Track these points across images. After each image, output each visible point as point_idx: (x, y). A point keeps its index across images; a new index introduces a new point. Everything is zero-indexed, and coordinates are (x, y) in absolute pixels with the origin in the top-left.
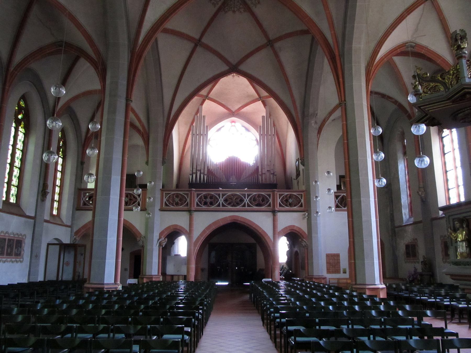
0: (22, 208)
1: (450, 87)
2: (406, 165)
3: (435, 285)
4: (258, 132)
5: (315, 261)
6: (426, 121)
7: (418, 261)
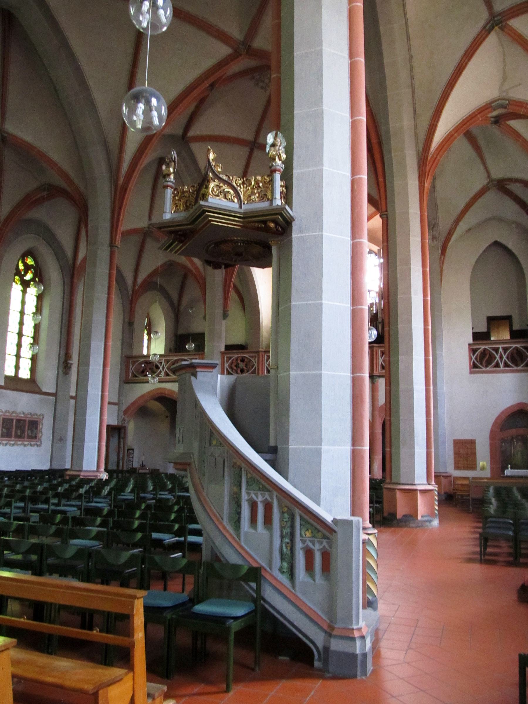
0: (37, 383)
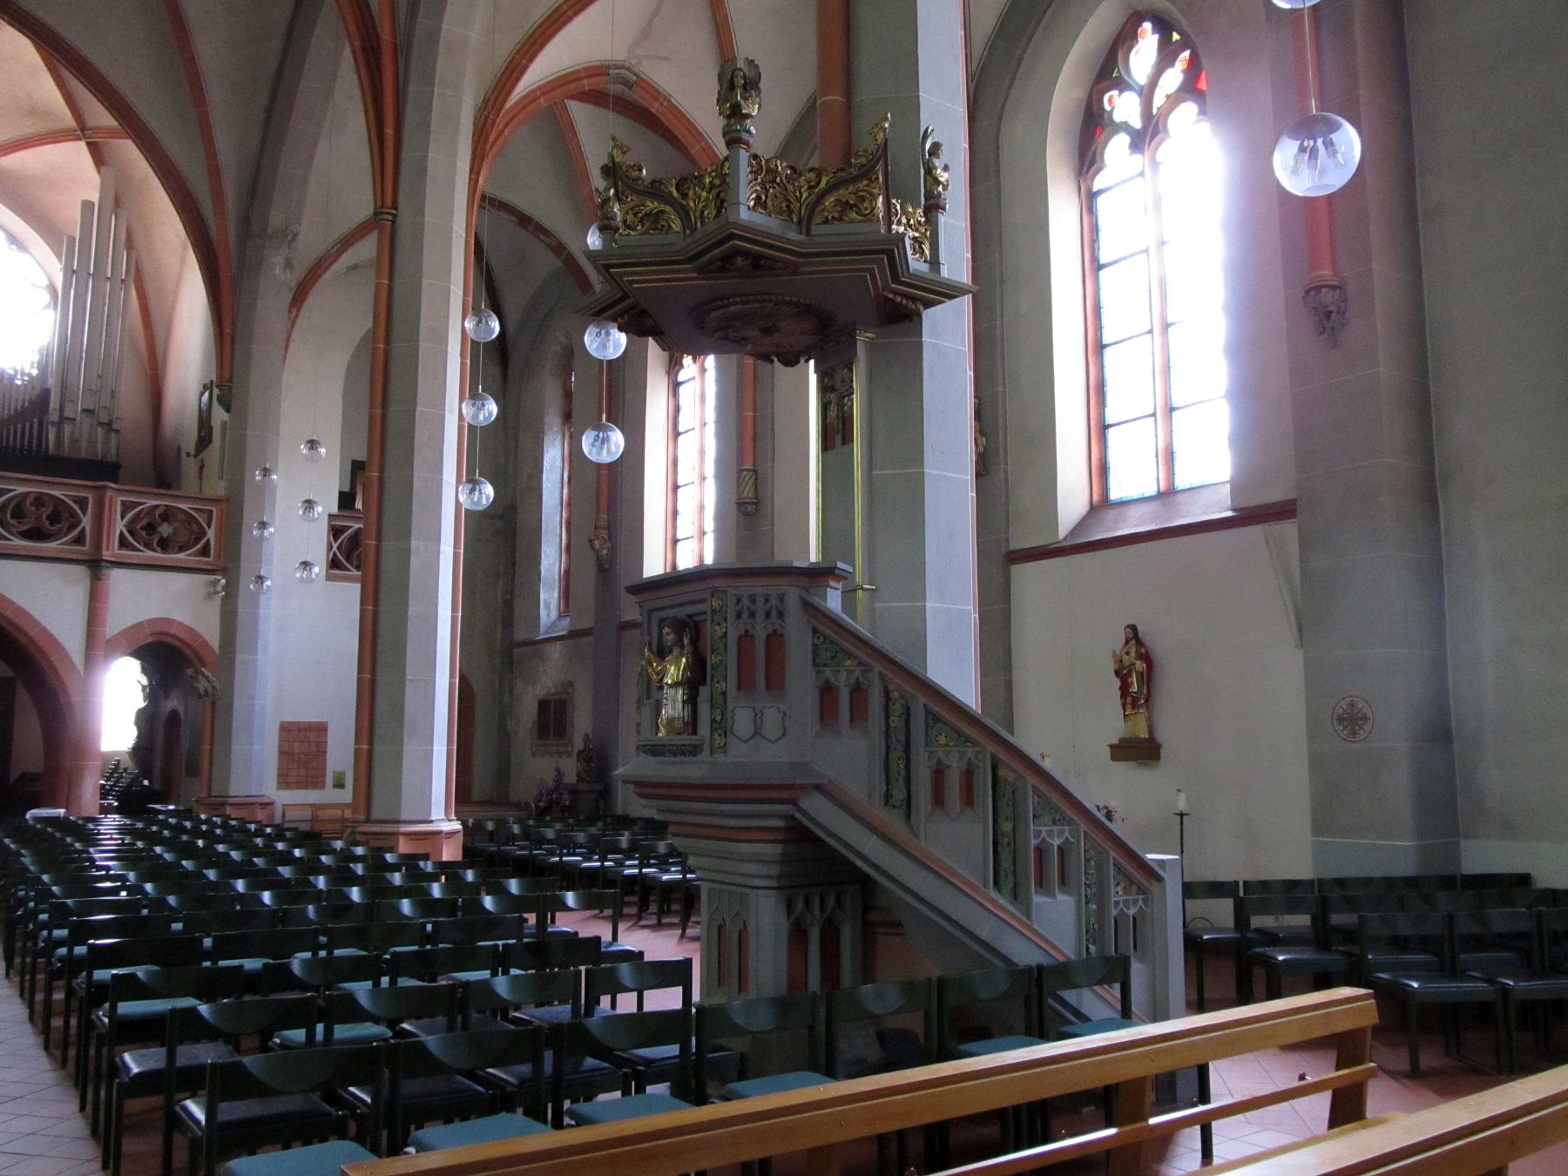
1: (699, 224)
2: (566, 451)
3: (609, 820)
4: (58, 256)
5: (236, 747)
6: (621, 315)
7: (570, 749)
